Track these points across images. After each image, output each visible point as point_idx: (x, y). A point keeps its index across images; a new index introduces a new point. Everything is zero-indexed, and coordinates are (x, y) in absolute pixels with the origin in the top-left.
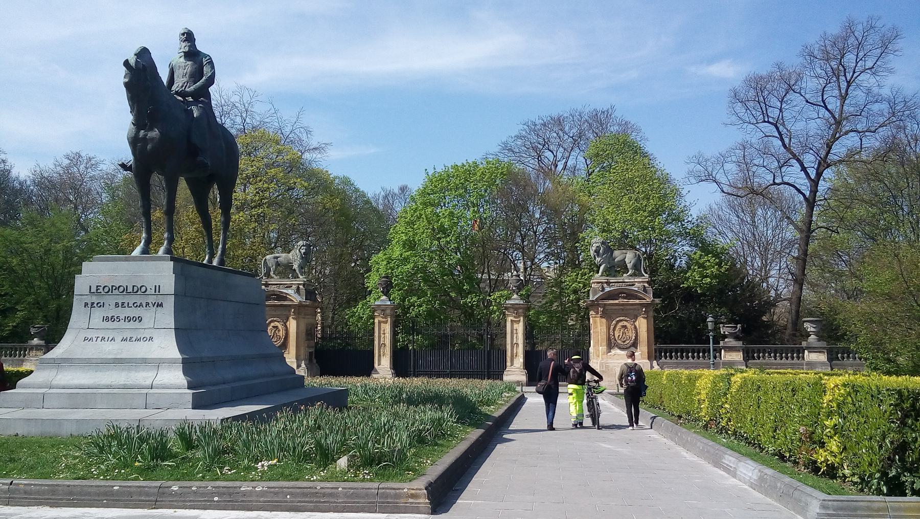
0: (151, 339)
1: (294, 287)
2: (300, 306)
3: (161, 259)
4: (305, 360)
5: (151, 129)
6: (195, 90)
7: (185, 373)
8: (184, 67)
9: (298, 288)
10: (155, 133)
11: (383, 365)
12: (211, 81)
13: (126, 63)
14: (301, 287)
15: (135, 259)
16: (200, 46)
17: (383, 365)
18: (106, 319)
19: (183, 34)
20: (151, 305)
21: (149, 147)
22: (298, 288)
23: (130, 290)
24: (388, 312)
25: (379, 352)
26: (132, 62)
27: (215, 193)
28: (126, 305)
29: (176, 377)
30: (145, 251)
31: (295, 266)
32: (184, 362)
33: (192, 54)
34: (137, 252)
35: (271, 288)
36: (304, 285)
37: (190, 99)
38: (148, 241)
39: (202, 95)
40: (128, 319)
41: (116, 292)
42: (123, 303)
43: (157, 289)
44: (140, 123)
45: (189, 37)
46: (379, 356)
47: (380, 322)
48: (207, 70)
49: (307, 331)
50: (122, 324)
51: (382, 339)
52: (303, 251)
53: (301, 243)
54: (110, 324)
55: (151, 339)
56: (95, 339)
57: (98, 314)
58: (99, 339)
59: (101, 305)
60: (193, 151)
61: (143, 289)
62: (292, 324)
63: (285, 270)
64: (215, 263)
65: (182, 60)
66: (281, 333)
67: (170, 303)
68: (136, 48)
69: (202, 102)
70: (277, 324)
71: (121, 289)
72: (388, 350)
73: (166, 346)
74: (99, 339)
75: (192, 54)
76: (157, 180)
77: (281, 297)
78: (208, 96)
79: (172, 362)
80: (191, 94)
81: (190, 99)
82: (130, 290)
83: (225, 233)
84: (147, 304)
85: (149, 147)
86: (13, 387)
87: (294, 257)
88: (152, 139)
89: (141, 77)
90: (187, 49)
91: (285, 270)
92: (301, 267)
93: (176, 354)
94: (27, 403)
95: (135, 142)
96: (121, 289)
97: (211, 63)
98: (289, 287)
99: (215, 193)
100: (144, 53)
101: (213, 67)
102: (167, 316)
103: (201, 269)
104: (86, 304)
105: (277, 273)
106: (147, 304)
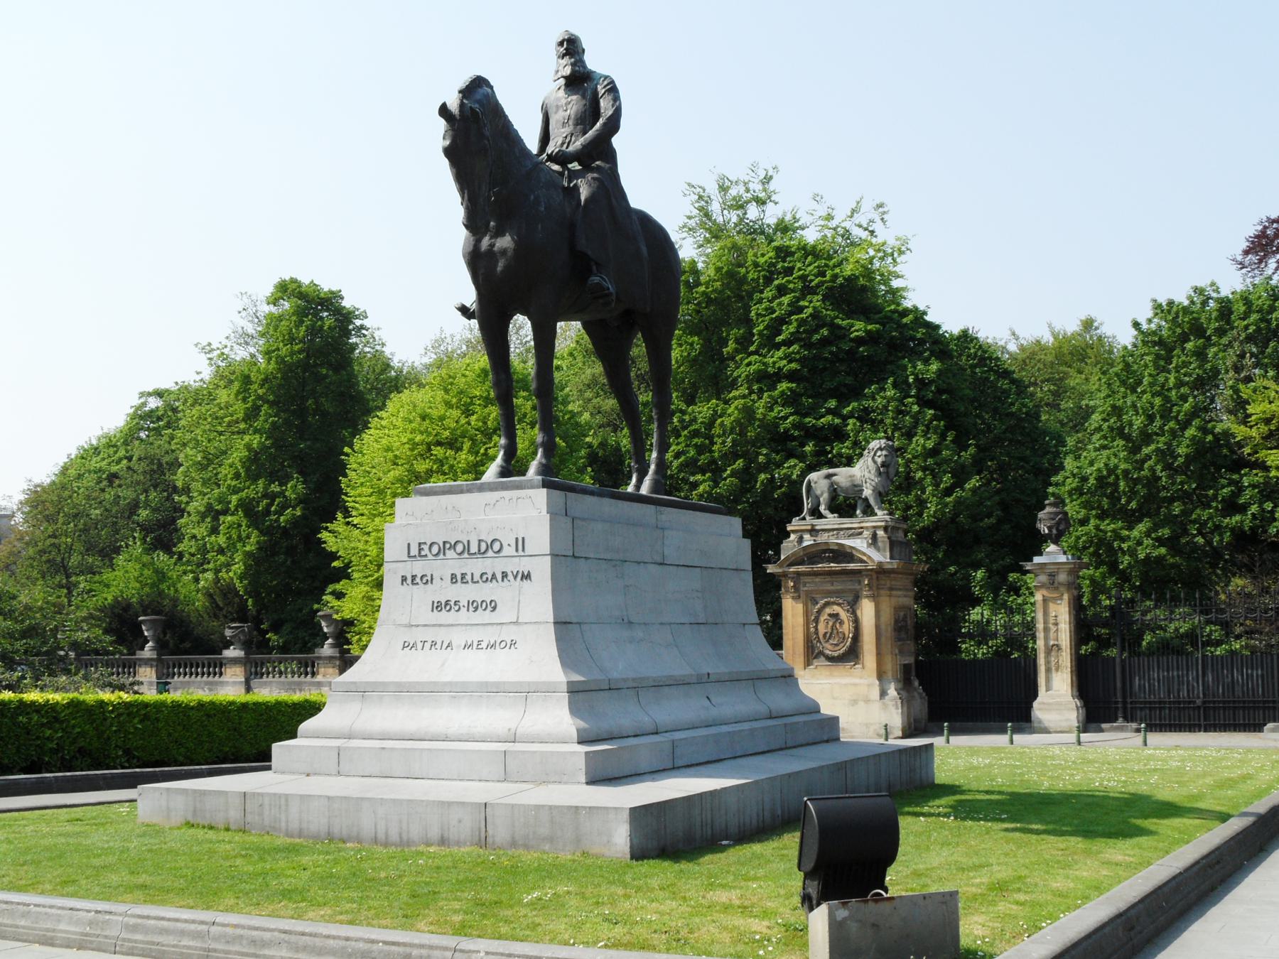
0: (513, 643)
1: (866, 534)
2: (881, 571)
3: (531, 486)
4: (897, 680)
5: (499, 233)
6: (585, 147)
7: (575, 710)
8: (568, 106)
9: (874, 537)
10: (505, 242)
11: (1056, 697)
12: (613, 125)
13: (444, 111)
14: (881, 533)
15: (492, 487)
16: (592, 62)
17: (1056, 697)
18: (438, 606)
19: (561, 44)
20: (511, 577)
21: (500, 266)
22: (874, 537)
23: (474, 549)
24: (1062, 577)
25: (1048, 662)
26: (453, 104)
27: (639, 349)
28: (468, 578)
29: (557, 719)
30: (505, 472)
31: (868, 492)
32: (574, 691)
33: (579, 80)
34: (491, 472)
35: (822, 538)
36: (886, 529)
37: (575, 166)
38: (511, 451)
39: (600, 154)
40: (474, 606)
41: (450, 554)
42: (463, 576)
43: (520, 544)
44: (474, 223)
45: (571, 47)
46: (1048, 670)
47: (1045, 600)
48: (606, 106)
49: (896, 621)
50: (464, 616)
51: (1052, 635)
52: (879, 460)
53: (874, 444)
54: (444, 617)
55: (513, 643)
56: (420, 645)
57: (423, 596)
58: (427, 645)
59: (427, 580)
60: (582, 266)
61: (496, 546)
62: (867, 610)
63: (845, 504)
64: (644, 490)
65: (562, 93)
66: (847, 628)
67: (542, 569)
68: (463, 80)
69: (598, 169)
70: (837, 609)
71: (459, 548)
72: (1066, 659)
73: (539, 659)
74: (427, 645)
75: (579, 80)
76: (521, 330)
77: (843, 555)
78: (610, 156)
79: (546, 689)
80: (576, 157)
81: (575, 166)
82: (474, 549)
83: (662, 428)
84: (504, 575)
85: (500, 266)
86: (293, 735)
87: (862, 473)
88: (504, 252)
89: (475, 131)
90: (568, 71)
91: (845, 504)
92: (881, 496)
93: (556, 674)
94: (340, 764)
95: (478, 262)
96: (459, 548)
97: (613, 90)
98: (857, 533)
99: (639, 349)
100: (477, 89)
101: (616, 98)
102: (536, 602)
103: (636, 506)
104: (404, 579)
105: (832, 509)
106: (504, 575)
